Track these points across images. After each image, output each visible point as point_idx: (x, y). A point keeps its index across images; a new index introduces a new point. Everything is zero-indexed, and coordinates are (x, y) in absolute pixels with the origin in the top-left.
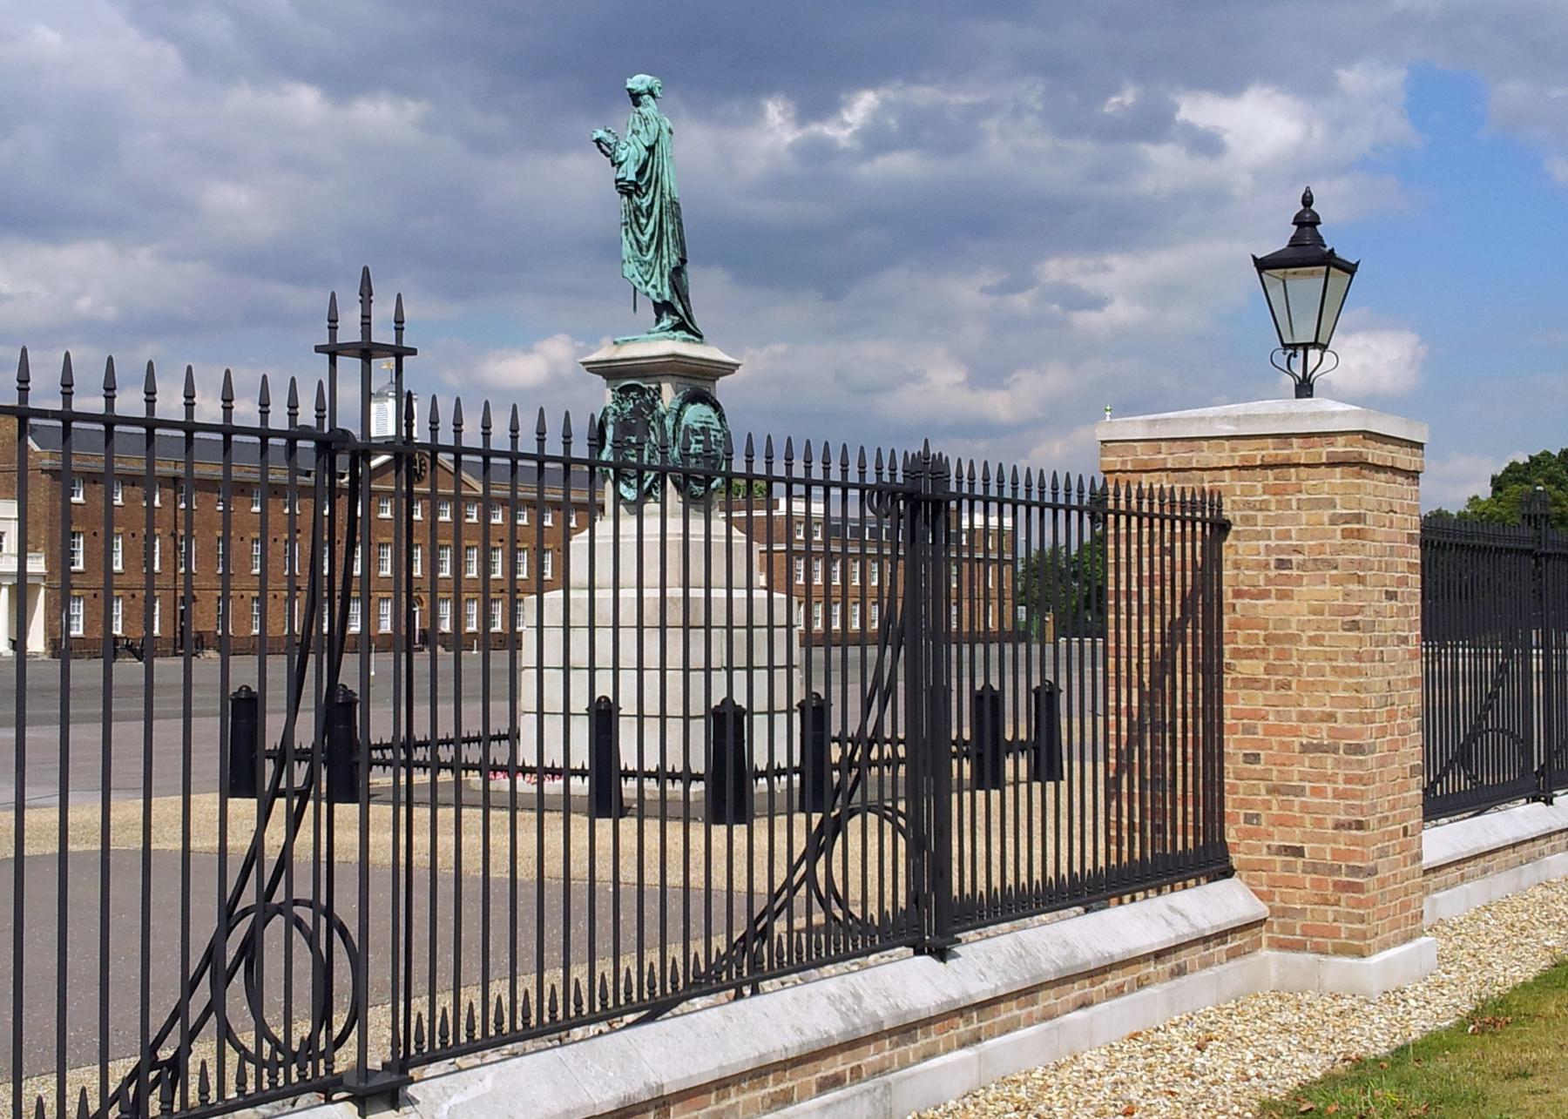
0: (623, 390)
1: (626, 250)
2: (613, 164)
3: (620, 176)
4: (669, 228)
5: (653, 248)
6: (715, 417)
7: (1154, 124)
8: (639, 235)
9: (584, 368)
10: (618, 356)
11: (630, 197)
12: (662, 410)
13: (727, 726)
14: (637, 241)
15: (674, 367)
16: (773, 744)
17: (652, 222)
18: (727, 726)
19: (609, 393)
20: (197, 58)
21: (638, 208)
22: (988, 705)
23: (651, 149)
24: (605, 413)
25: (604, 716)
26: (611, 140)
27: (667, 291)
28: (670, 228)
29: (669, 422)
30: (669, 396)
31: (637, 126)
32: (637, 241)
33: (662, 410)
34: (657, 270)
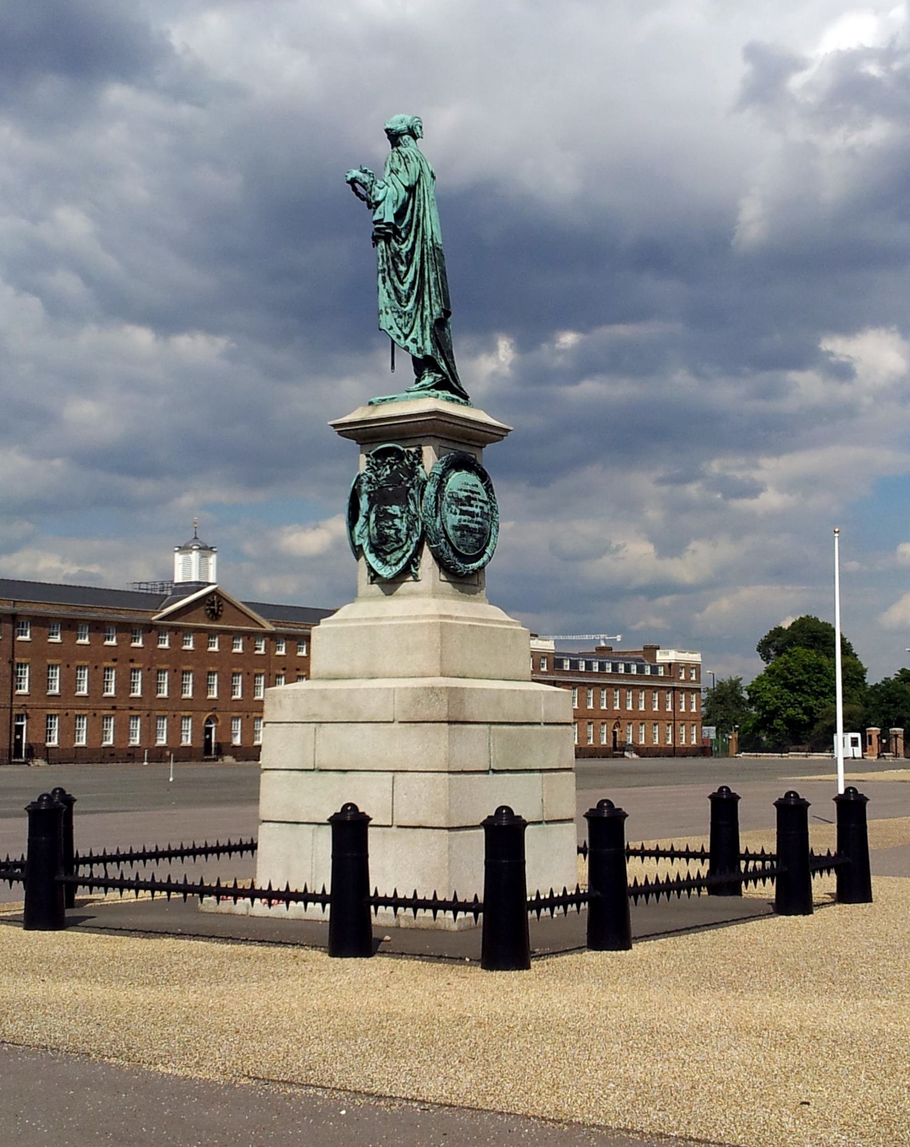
0: (377, 455)
1: (384, 299)
2: (370, 207)
3: (377, 217)
4: (431, 276)
5: (413, 299)
6: (481, 488)
7: (803, 357)
8: (397, 284)
9: (334, 431)
10: (374, 416)
11: (388, 242)
12: (422, 475)
13: (505, 837)
14: (396, 289)
15: (434, 427)
16: (555, 865)
17: (412, 270)
18: (505, 837)
19: (363, 459)
20: (57, 309)
21: (397, 254)
22: (792, 814)
23: (411, 190)
24: (359, 481)
25: (350, 832)
26: (366, 179)
27: (428, 344)
28: (433, 276)
29: (430, 489)
30: (430, 460)
31: (396, 165)
32: (396, 289)
33: (422, 475)
34: (418, 322)
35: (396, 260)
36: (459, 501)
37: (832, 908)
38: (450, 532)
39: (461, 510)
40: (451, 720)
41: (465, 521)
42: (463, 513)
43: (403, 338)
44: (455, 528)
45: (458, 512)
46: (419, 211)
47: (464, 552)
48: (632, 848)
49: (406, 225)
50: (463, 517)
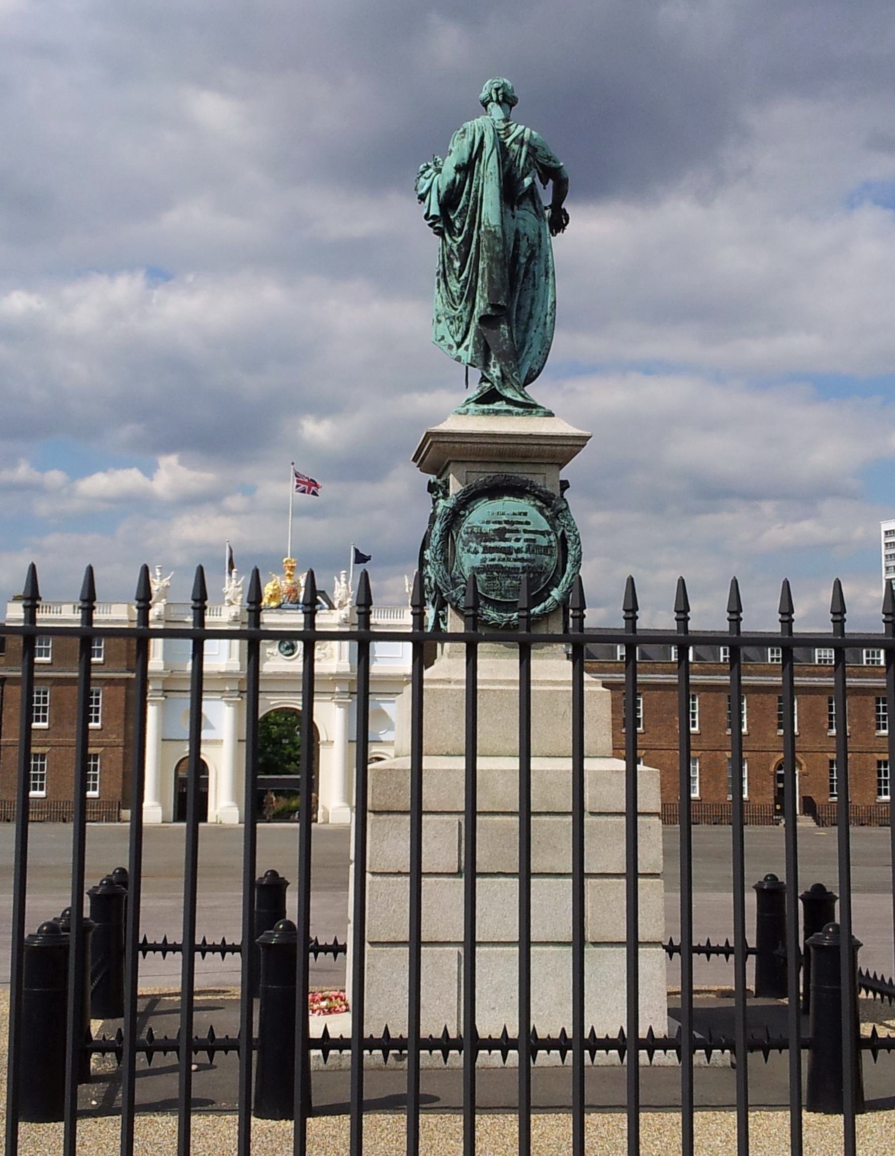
35: (452, 256)
36: (483, 537)
37: (165, 990)
39: (485, 548)
40: (377, 809)
41: (493, 560)
42: (487, 550)
43: (455, 347)
45: (481, 550)
46: (477, 191)
47: (498, 598)
48: (321, 943)
49: (460, 213)
50: (488, 556)
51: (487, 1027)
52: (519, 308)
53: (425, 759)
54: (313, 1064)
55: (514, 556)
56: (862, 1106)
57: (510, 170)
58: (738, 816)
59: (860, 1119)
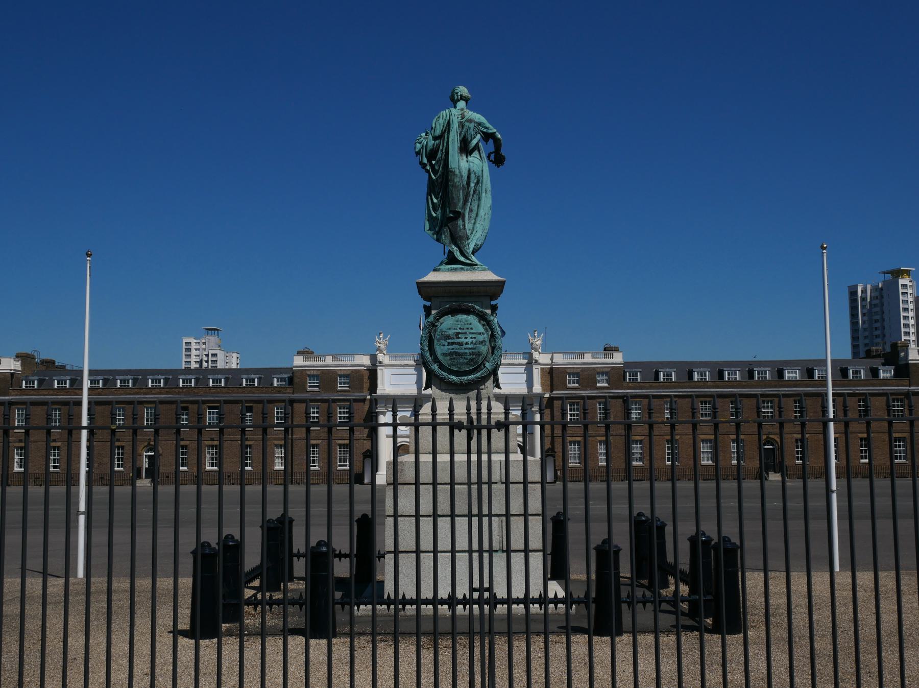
38: (441, 358)
42: (449, 344)
44: (445, 355)
51: (459, 596)
52: (471, 211)
53: (456, 455)
54: (550, 611)
55: (465, 346)
56: (335, 636)
57: (464, 137)
58: (243, 479)
59: (334, 641)
